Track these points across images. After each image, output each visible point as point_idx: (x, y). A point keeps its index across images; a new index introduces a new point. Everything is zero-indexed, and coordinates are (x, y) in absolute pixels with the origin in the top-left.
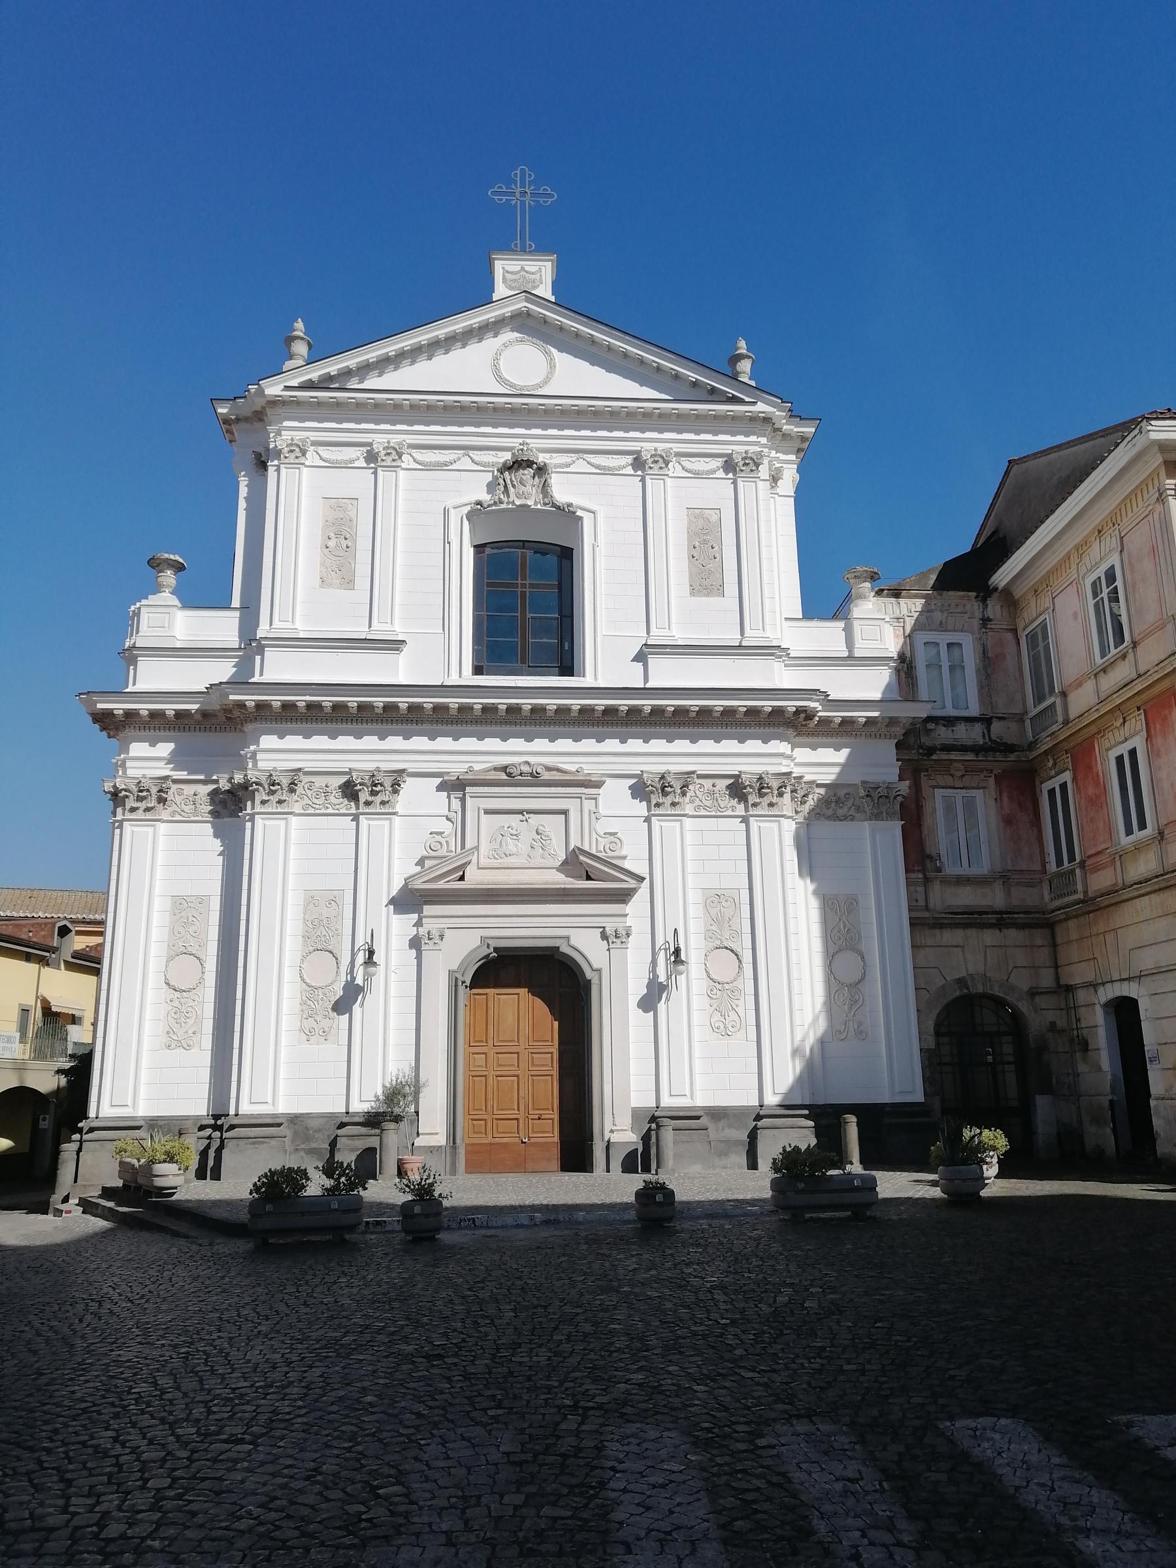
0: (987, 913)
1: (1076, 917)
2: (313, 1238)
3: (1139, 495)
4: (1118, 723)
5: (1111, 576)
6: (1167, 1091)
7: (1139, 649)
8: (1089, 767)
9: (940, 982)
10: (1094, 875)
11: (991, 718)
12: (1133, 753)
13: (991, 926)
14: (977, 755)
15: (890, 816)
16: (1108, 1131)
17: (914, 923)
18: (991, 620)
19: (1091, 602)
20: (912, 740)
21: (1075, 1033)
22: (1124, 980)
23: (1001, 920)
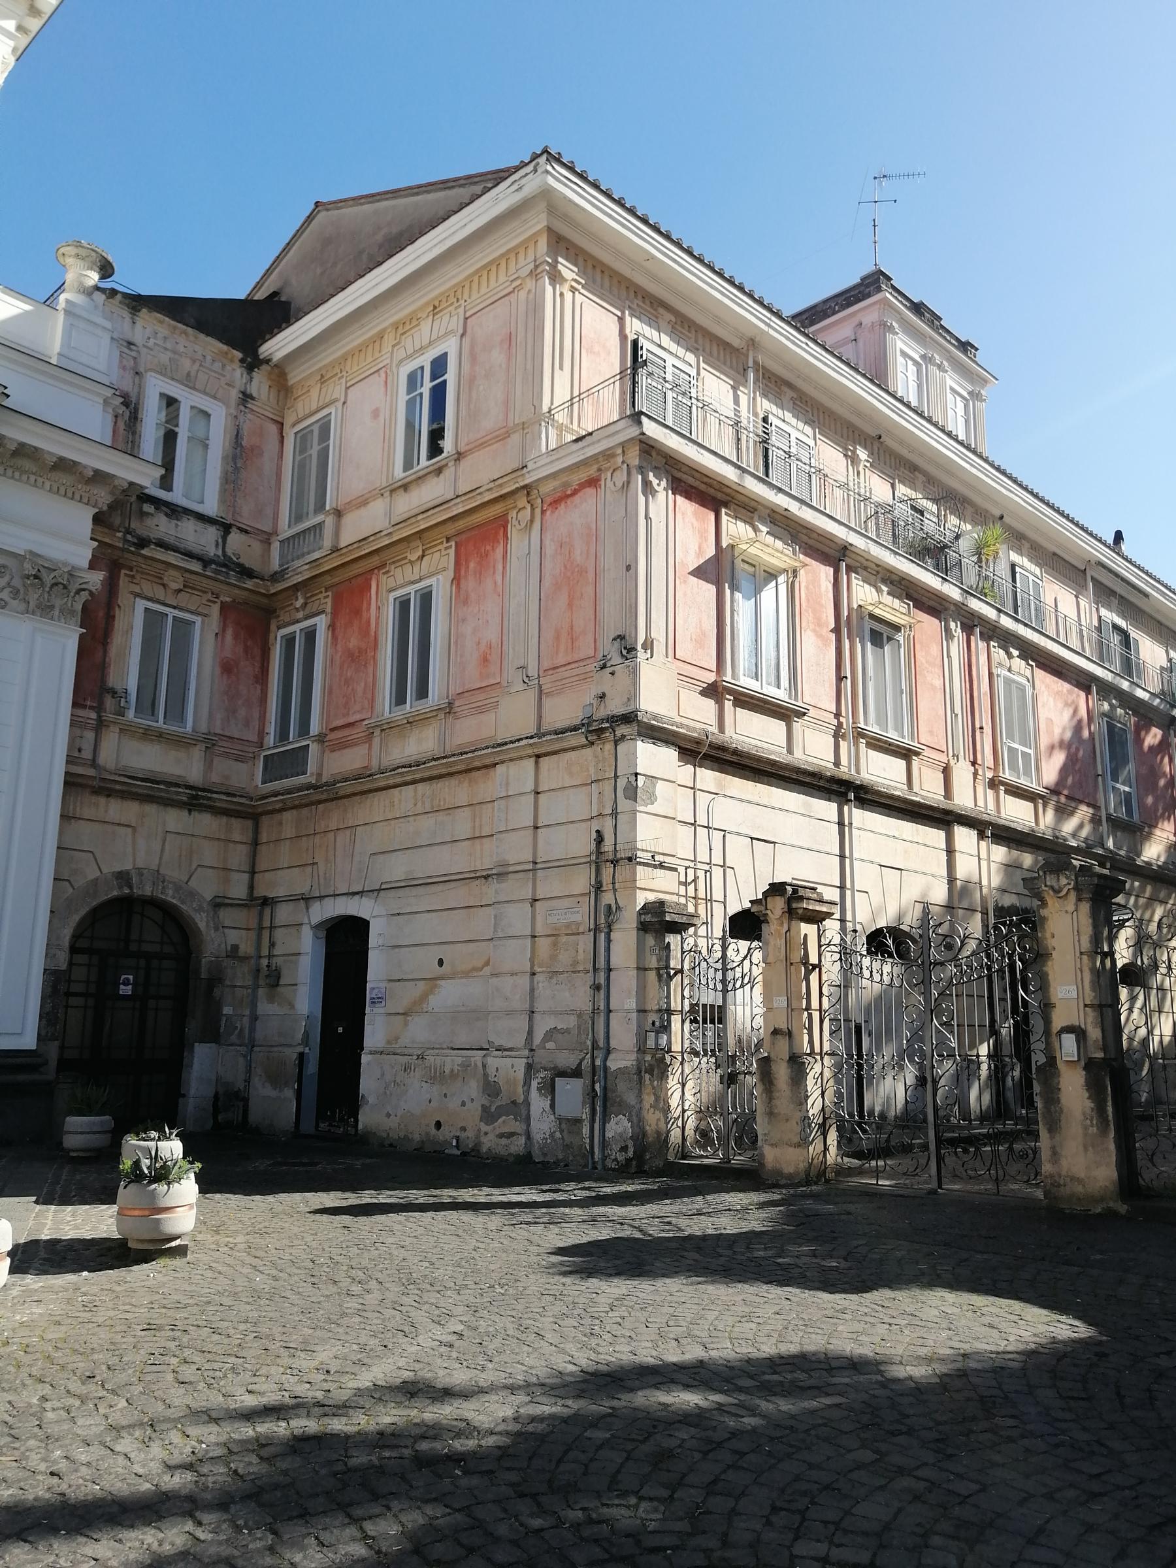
0: (177, 785)
1: (295, 807)
2: (902, 650)
3: (485, 277)
4: (413, 557)
5: (439, 365)
6: (389, 1042)
7: (465, 464)
8: (357, 612)
9: (92, 873)
10: (336, 754)
11: (230, 526)
12: (426, 598)
13: (180, 805)
14: (205, 567)
15: (66, 613)
16: (289, 1093)
17: (72, 783)
18: (253, 398)
19: (403, 397)
20: (117, 520)
21: (265, 962)
22: (357, 893)
23: (196, 799)
